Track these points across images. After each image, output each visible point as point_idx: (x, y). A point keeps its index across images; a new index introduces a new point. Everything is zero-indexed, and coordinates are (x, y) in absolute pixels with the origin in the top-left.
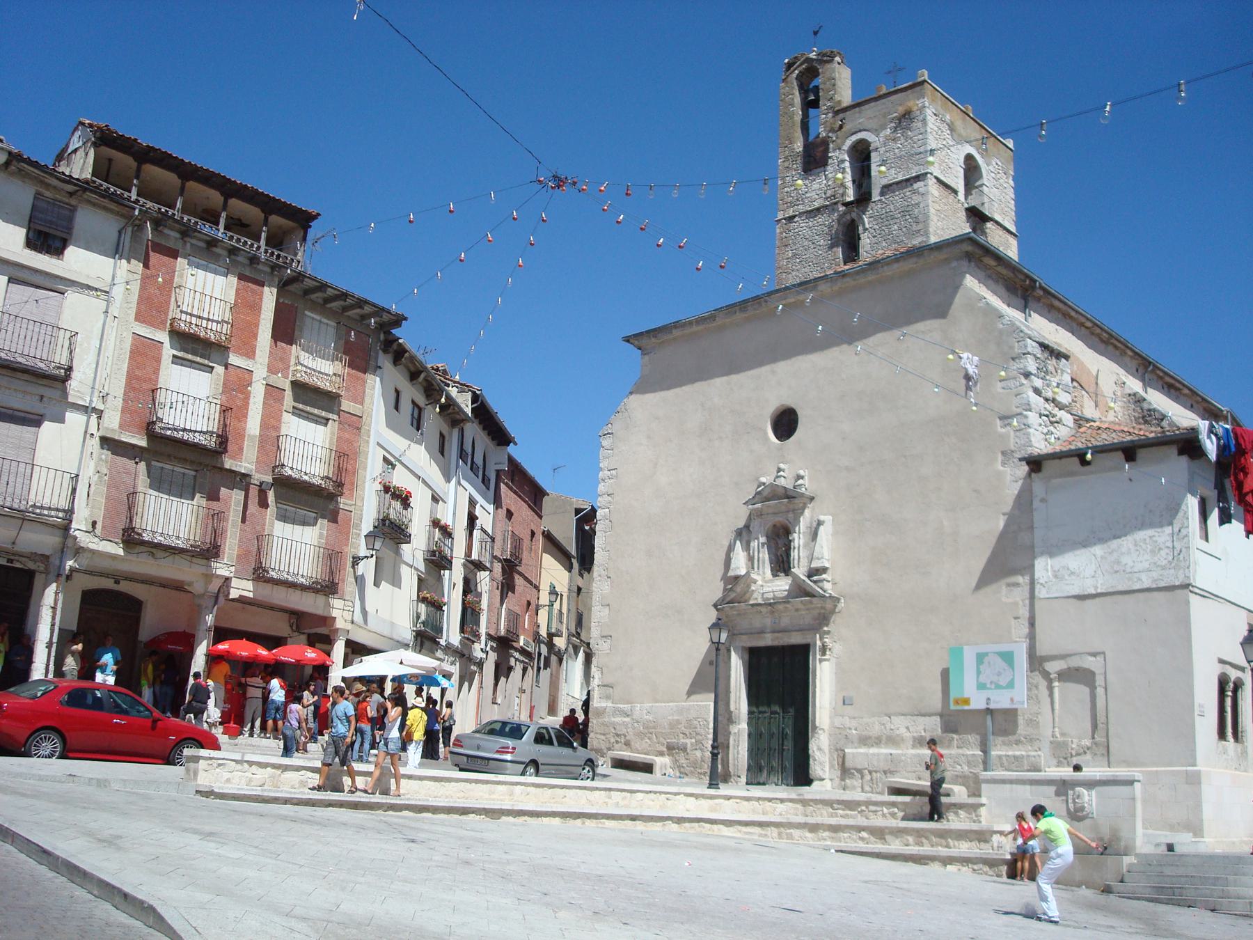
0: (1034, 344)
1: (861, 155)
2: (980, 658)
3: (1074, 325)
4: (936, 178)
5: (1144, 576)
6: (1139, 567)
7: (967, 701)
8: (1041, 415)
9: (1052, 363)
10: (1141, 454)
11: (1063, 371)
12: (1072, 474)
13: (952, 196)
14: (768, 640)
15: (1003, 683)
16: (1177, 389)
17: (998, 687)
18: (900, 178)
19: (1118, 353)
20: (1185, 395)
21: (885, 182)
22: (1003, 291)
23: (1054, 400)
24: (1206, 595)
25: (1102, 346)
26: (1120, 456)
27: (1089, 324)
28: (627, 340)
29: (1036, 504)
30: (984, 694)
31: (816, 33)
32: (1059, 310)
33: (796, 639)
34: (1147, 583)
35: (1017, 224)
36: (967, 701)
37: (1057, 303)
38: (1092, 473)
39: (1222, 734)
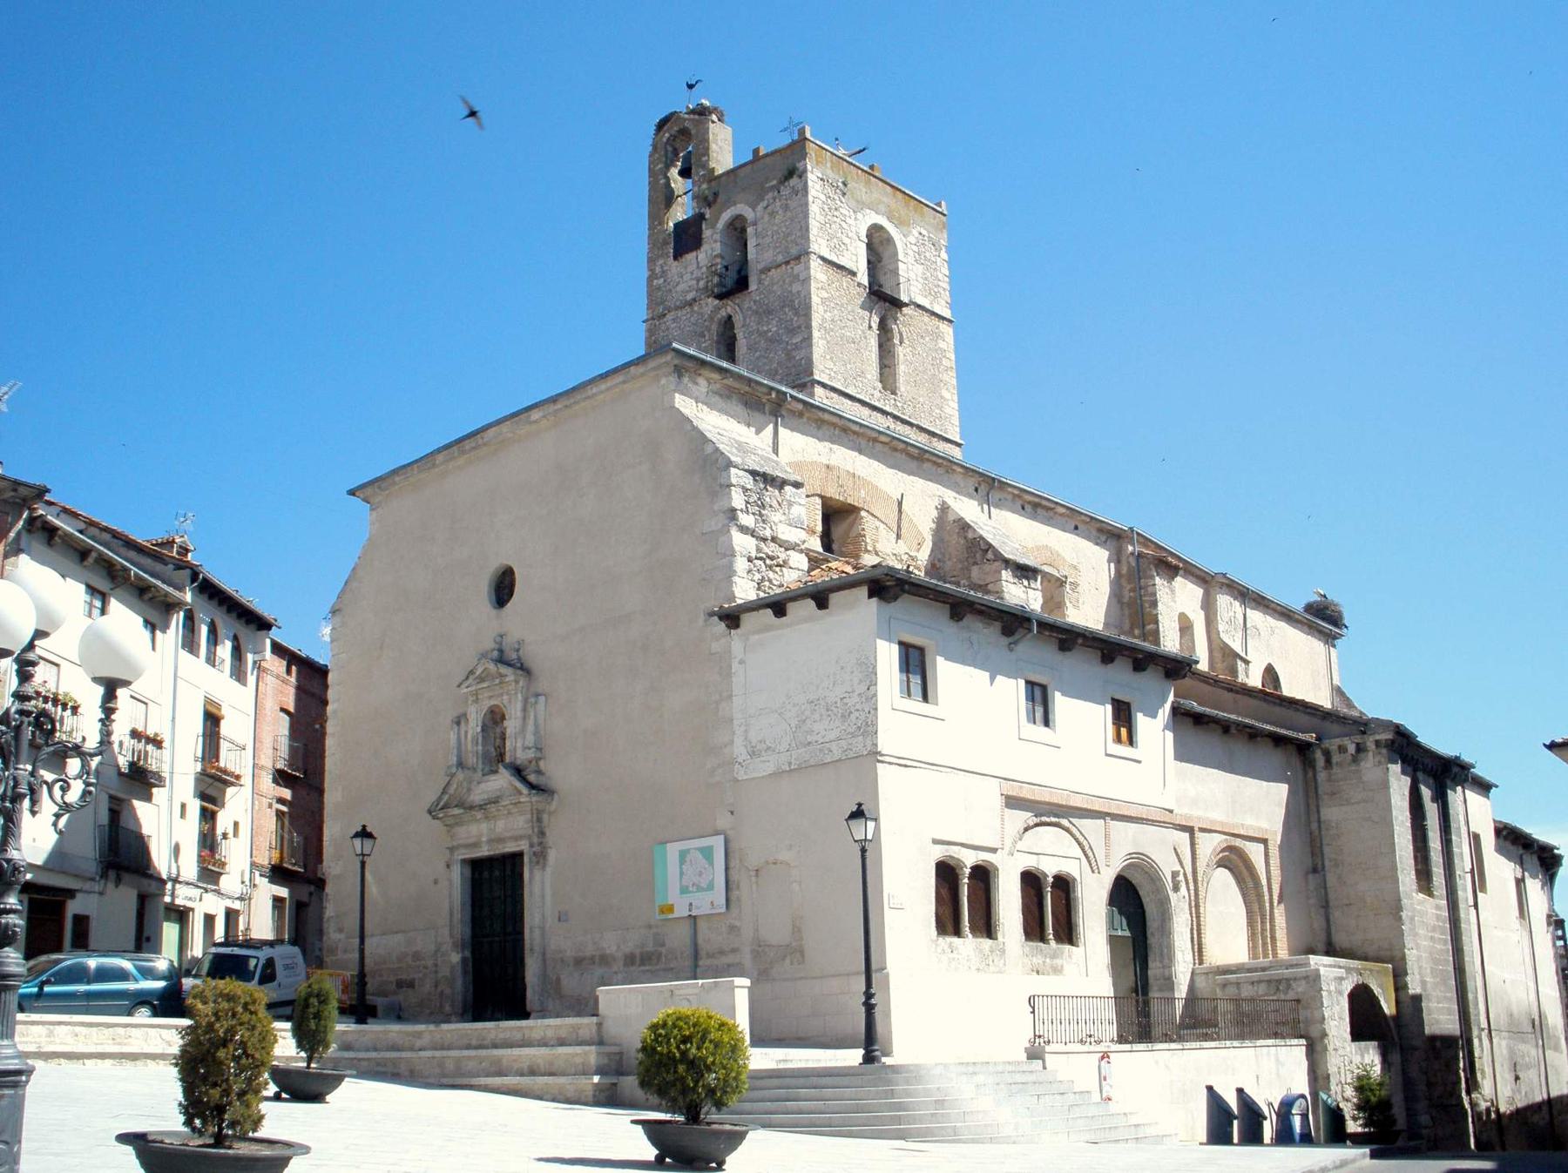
0: (741, 473)
1: (738, 229)
2: (683, 855)
3: (864, 443)
4: (823, 259)
5: (834, 746)
6: (832, 735)
7: (671, 909)
8: (750, 560)
9: (771, 495)
10: (835, 598)
11: (790, 504)
12: (768, 628)
13: (846, 281)
14: (484, 852)
15: (704, 885)
16: (1048, 509)
17: (700, 889)
18: (780, 258)
19: (941, 471)
20: (1062, 515)
21: (760, 267)
22: (740, 409)
23: (774, 539)
24: (903, 763)
25: (914, 465)
26: (811, 603)
27: (883, 438)
28: (352, 493)
29: (735, 666)
30: (687, 898)
31: (690, 87)
32: (835, 425)
33: (510, 848)
34: (837, 754)
35: (951, 306)
36: (671, 909)
37: (826, 417)
38: (788, 626)
39: (948, 923)
